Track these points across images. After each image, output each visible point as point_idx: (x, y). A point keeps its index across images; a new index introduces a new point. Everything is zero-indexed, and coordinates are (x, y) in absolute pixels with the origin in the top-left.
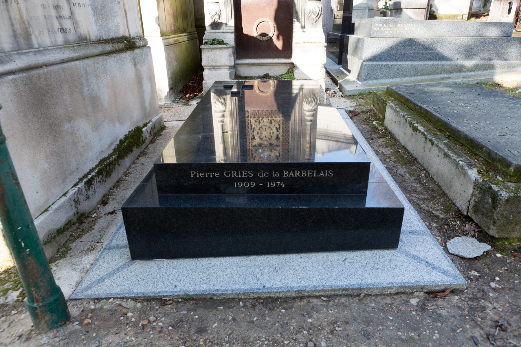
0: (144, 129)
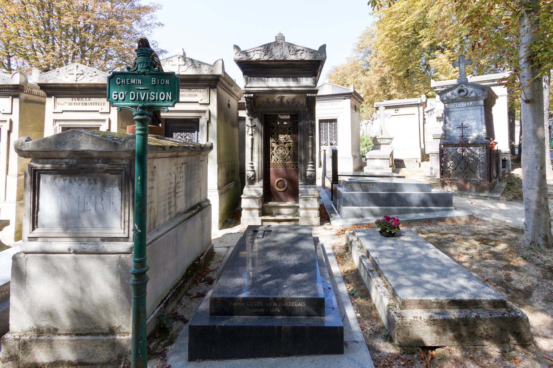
0: (201, 258)
